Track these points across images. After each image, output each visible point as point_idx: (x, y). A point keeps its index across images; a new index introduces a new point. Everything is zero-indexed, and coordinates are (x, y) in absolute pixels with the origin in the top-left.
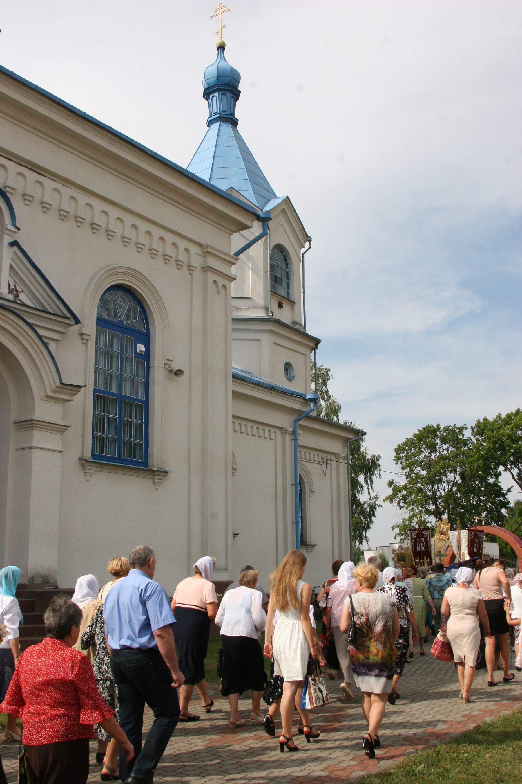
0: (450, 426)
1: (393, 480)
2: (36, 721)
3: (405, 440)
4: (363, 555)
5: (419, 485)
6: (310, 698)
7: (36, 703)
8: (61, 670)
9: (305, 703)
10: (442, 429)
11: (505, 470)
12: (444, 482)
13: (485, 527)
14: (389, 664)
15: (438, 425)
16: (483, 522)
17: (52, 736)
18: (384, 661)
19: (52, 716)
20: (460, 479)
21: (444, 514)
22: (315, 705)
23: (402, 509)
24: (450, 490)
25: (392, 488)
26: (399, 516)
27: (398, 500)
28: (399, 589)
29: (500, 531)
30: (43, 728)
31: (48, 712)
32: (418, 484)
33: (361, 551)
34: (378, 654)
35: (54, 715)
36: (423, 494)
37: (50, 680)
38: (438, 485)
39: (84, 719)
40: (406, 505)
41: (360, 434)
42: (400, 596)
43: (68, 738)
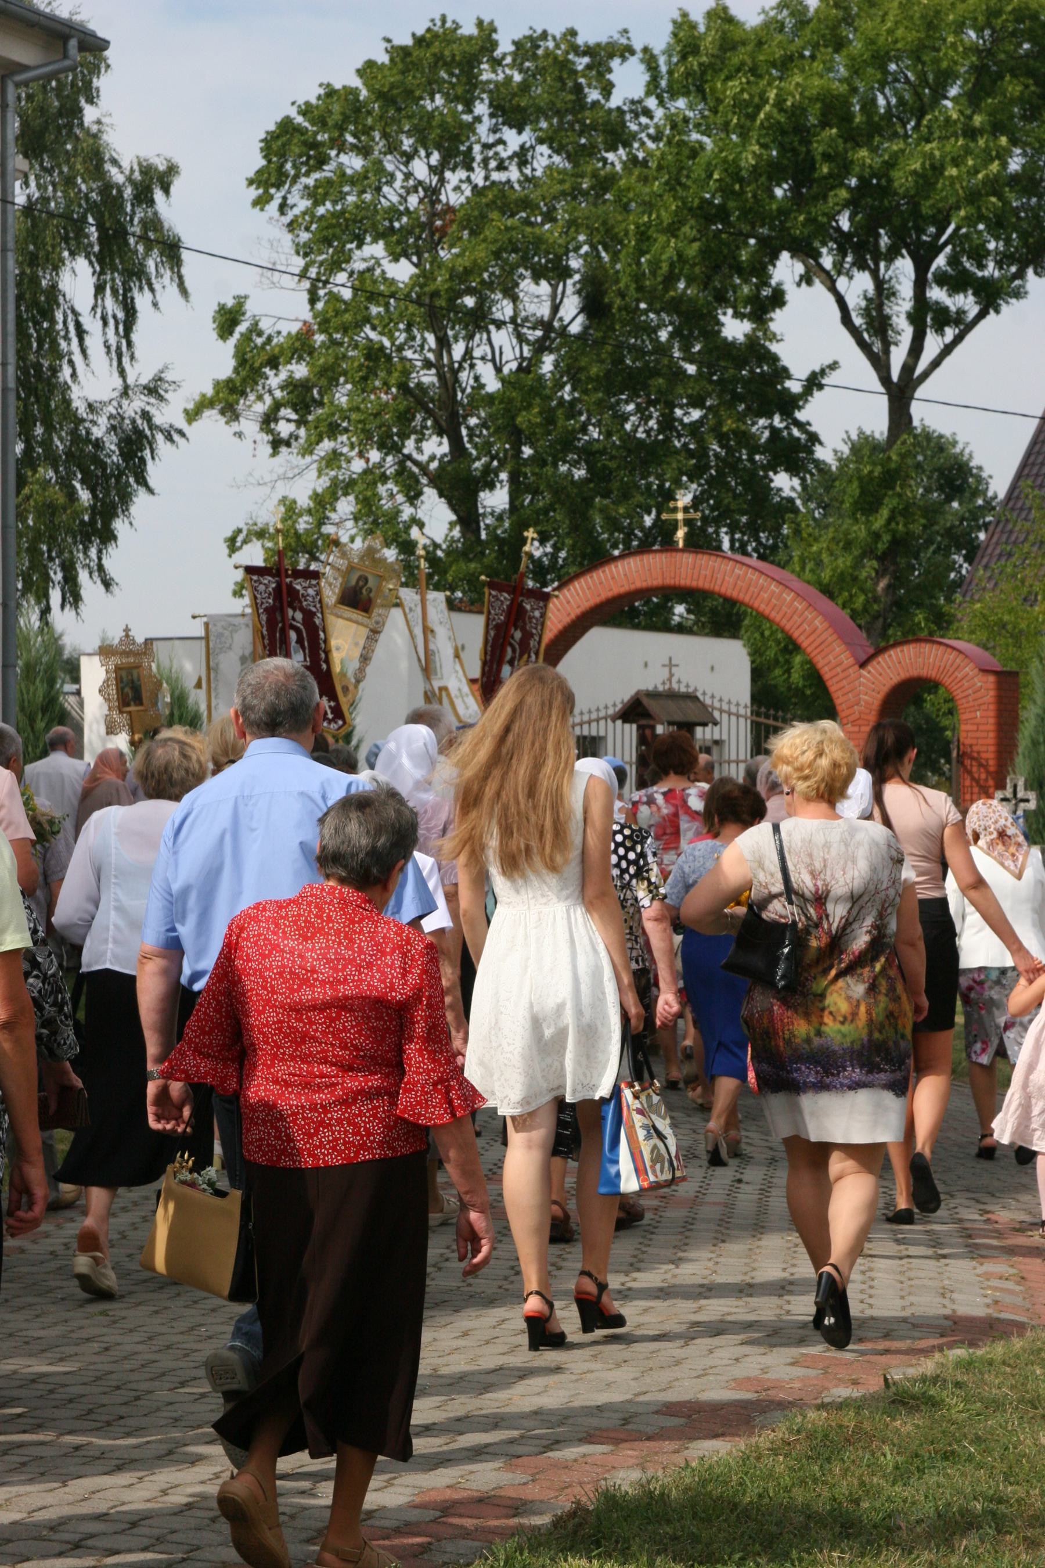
0: (544, 35)
1: (241, 301)
2: (297, 1106)
3: (311, 94)
4: (76, 680)
5: (373, 335)
6: (636, 1155)
7: (293, 1058)
8: (373, 976)
9: (618, 1175)
10: (505, 46)
11: (806, 279)
12: (499, 324)
13: (688, 558)
14: (891, 1044)
15: (487, 31)
16: (680, 534)
17: (354, 1146)
18: (876, 1035)
19: (347, 1095)
20: (582, 310)
21: (491, 486)
22: (652, 1178)
23: (283, 450)
24: (527, 367)
25: (233, 341)
26: (266, 490)
27: (260, 408)
28: (621, 832)
29: (762, 580)
30: (321, 1123)
31: (337, 1084)
32: (367, 329)
33: (66, 655)
34: (854, 1014)
35: (353, 1092)
36: (396, 375)
37: (346, 998)
38: (470, 337)
39: (304, 1134)
40: (302, 432)
41: (73, 43)
42: (625, 857)
43: (393, 1149)
